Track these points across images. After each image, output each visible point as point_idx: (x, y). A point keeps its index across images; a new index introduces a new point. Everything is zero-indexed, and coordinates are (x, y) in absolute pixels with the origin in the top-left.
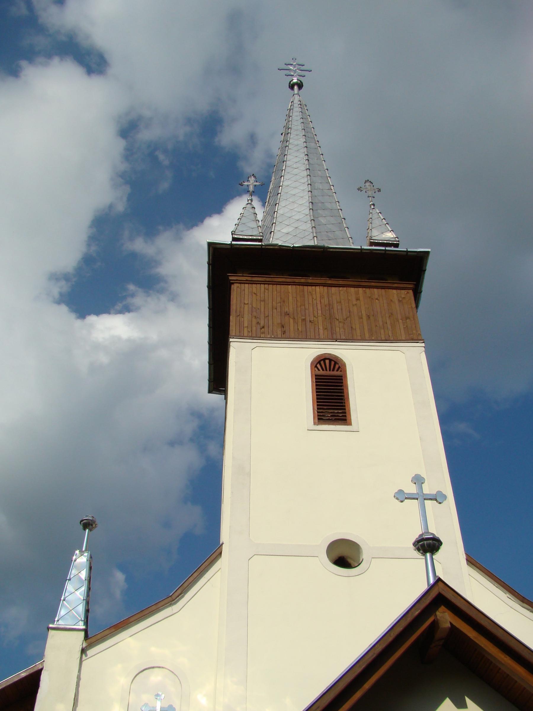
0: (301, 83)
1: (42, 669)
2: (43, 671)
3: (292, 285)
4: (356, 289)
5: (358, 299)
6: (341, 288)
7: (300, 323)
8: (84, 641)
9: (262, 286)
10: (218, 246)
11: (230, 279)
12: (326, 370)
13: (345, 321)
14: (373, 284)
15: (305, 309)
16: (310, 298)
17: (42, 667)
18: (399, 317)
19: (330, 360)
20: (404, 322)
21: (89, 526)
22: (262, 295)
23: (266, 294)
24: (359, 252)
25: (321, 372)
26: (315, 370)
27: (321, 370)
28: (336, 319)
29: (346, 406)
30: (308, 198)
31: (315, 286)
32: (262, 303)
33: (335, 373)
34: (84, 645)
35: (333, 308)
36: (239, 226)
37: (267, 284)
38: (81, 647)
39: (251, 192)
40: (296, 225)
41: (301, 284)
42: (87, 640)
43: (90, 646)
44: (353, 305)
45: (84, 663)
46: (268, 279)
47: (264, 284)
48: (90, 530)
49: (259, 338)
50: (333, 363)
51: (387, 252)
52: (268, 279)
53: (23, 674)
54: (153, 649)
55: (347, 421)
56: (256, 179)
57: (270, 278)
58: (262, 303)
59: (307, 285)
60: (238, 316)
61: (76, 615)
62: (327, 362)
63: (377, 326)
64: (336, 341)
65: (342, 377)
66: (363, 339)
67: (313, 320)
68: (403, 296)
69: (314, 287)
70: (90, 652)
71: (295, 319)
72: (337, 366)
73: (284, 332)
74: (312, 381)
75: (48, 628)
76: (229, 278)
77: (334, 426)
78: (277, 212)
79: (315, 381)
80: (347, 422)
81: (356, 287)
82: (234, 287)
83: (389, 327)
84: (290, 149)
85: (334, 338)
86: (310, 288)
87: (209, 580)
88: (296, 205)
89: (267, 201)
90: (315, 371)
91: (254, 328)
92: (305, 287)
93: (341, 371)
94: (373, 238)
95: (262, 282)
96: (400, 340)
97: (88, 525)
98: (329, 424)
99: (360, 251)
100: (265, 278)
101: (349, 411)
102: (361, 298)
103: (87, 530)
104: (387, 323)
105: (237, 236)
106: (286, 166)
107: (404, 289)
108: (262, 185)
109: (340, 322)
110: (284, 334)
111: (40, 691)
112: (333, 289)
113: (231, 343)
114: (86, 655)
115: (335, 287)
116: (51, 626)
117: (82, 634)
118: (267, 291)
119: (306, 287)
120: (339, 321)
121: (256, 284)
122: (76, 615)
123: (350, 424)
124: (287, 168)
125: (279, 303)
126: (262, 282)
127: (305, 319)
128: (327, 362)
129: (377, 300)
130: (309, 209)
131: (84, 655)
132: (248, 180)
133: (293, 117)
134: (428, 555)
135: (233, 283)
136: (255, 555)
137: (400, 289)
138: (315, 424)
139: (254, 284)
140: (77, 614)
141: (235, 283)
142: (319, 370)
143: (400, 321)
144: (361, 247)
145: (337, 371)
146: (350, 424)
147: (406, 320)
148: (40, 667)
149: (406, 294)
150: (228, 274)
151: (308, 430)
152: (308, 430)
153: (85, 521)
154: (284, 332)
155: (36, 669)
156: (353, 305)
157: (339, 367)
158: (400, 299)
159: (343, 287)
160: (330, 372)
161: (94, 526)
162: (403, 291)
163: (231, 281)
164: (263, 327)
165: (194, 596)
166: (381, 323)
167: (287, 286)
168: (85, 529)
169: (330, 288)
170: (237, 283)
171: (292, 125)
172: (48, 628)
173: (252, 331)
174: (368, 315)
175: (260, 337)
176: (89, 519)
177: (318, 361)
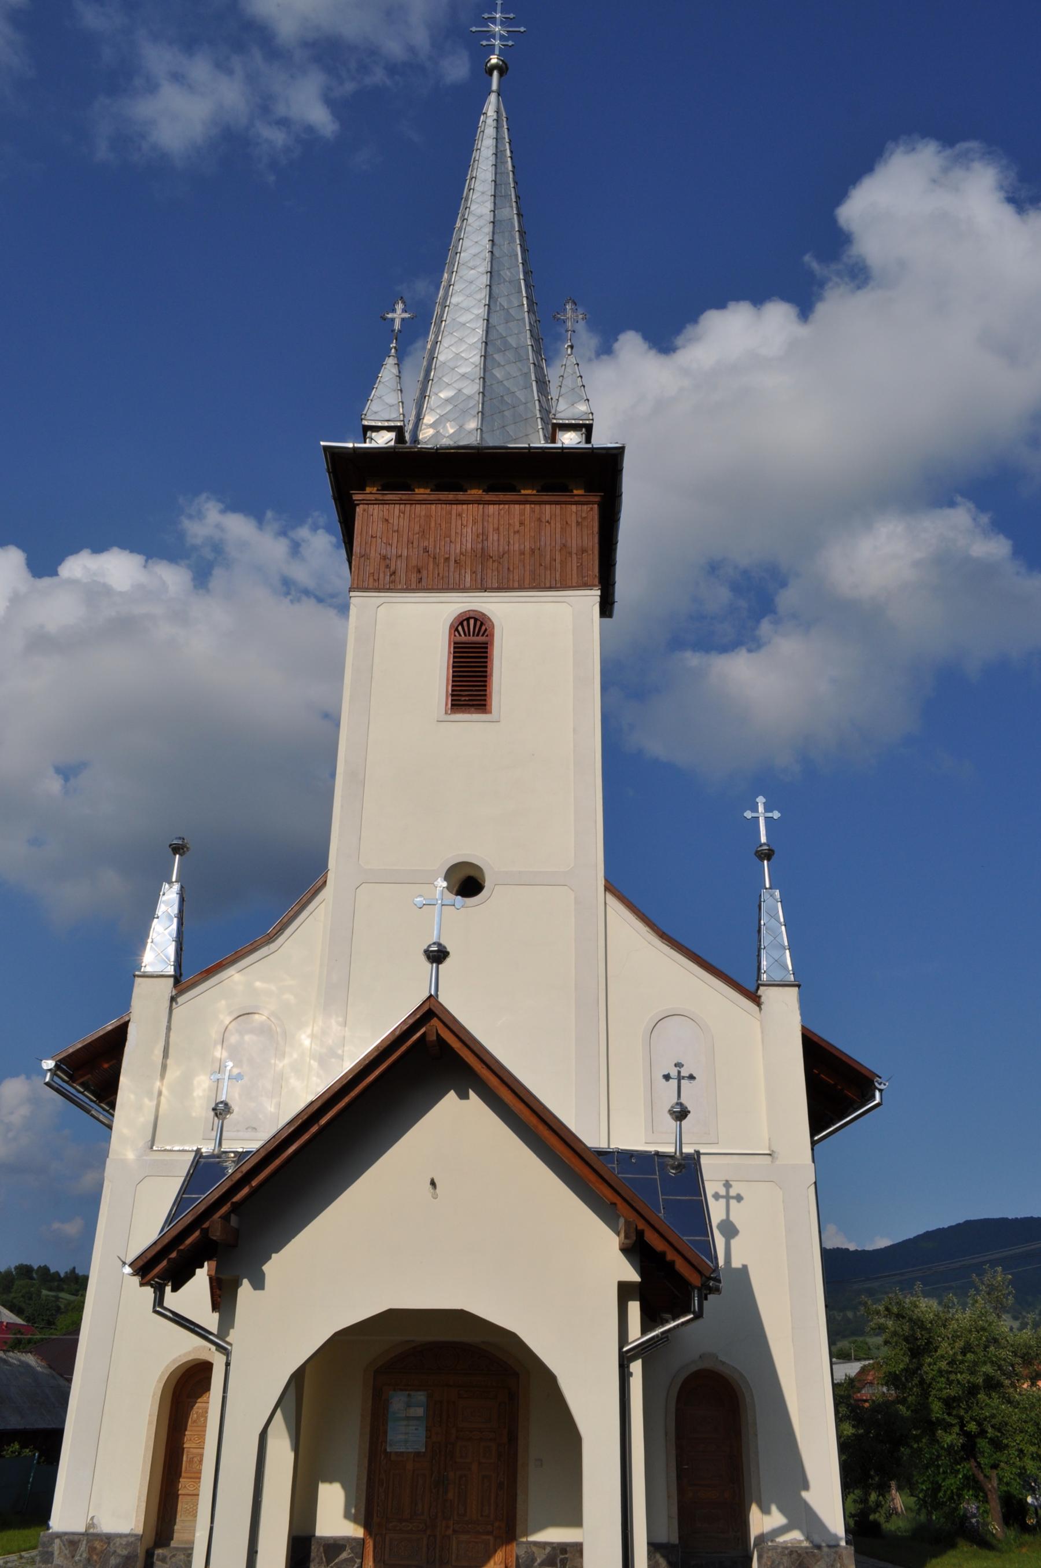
0: (504, 66)
1: (129, 1021)
2: (130, 1024)
3: (436, 504)
4: (522, 506)
5: (522, 523)
6: (502, 506)
7: (441, 565)
8: (173, 989)
9: (397, 506)
10: (336, 450)
11: (354, 498)
12: (469, 635)
13: (500, 558)
14: (545, 498)
15: (451, 542)
16: (459, 522)
17: (129, 1019)
18: (574, 550)
19: (476, 620)
20: (579, 557)
21: (179, 851)
22: (396, 522)
23: (401, 520)
24: (88, 1092)
25: (463, 638)
26: (455, 636)
27: (463, 635)
28: (490, 556)
29: (488, 686)
30: (481, 333)
31: (468, 504)
32: (396, 534)
33: (480, 639)
34: (174, 993)
35: (487, 539)
36: (373, 402)
37: (403, 504)
38: (170, 995)
39: (396, 331)
40: (458, 385)
41: (448, 502)
42: (178, 988)
43: (181, 993)
44: (515, 533)
45: (174, 1011)
46: (404, 497)
47: (400, 504)
48: (181, 855)
49: (390, 590)
50: (478, 623)
51: (565, 451)
52: (404, 497)
53: (109, 1026)
54: (258, 984)
55: (487, 707)
56: (405, 306)
57: (407, 495)
58: (396, 534)
59: (457, 504)
60: (363, 556)
61: (165, 959)
62: (472, 622)
63: (542, 565)
64: (485, 591)
65: (487, 644)
66: (521, 588)
67: (460, 560)
68: (584, 515)
69: (465, 507)
70: (180, 1000)
71: (435, 558)
72: (483, 628)
73: (420, 580)
74: (449, 652)
75: (135, 976)
76: (352, 498)
77: (469, 715)
78: (437, 358)
79: (452, 652)
80: (486, 709)
81: (523, 504)
82: (359, 510)
83: (558, 566)
84: (469, 225)
85: (482, 587)
86: (460, 507)
87: (311, 913)
88: (464, 347)
89: (434, 320)
90: (455, 638)
91: (381, 575)
92: (453, 506)
93: (487, 636)
94: (558, 416)
95: (397, 502)
96: (569, 587)
97: (177, 849)
98: (463, 712)
99: (527, 451)
100: (400, 496)
101: (491, 693)
102: (527, 522)
103: (177, 856)
104: (555, 560)
105: (368, 422)
106: (459, 263)
107: (587, 504)
108: (413, 319)
109: (494, 561)
110: (419, 582)
111: (127, 1044)
112: (491, 507)
113: (352, 598)
114: (177, 1003)
115: (494, 504)
116: (137, 973)
117: (172, 980)
118: (402, 515)
119: (454, 506)
120: (494, 559)
121: (389, 504)
122: (165, 959)
123: (490, 712)
124: (461, 267)
125: (417, 534)
126: (397, 502)
127: (449, 558)
128: (472, 622)
129: (547, 524)
130: (480, 355)
131: (174, 1003)
132: (393, 310)
133: (482, 149)
134: (434, 965)
135: (358, 505)
136: (364, 883)
137: (582, 504)
138: (446, 713)
139: (386, 504)
140: (533, 393)
141: (361, 504)
142: (460, 635)
143: (574, 556)
144: (529, 445)
145: (483, 635)
146: (490, 712)
147: (582, 554)
148: (127, 1019)
149: (589, 511)
150: (352, 492)
151: (438, 721)
152: (438, 721)
153: (174, 846)
154: (420, 580)
155: (122, 1021)
156: (515, 533)
157: (486, 630)
158: (580, 520)
159: (504, 504)
160: (473, 638)
161: (185, 849)
162: (585, 507)
163: (356, 502)
164: (394, 573)
165: (294, 932)
166: (548, 562)
167: (429, 506)
168: (175, 854)
169: (486, 506)
170: (363, 504)
171: (479, 169)
172: (135, 976)
173: (378, 579)
174: (533, 547)
175: (389, 589)
176: (179, 844)
177: (460, 621)
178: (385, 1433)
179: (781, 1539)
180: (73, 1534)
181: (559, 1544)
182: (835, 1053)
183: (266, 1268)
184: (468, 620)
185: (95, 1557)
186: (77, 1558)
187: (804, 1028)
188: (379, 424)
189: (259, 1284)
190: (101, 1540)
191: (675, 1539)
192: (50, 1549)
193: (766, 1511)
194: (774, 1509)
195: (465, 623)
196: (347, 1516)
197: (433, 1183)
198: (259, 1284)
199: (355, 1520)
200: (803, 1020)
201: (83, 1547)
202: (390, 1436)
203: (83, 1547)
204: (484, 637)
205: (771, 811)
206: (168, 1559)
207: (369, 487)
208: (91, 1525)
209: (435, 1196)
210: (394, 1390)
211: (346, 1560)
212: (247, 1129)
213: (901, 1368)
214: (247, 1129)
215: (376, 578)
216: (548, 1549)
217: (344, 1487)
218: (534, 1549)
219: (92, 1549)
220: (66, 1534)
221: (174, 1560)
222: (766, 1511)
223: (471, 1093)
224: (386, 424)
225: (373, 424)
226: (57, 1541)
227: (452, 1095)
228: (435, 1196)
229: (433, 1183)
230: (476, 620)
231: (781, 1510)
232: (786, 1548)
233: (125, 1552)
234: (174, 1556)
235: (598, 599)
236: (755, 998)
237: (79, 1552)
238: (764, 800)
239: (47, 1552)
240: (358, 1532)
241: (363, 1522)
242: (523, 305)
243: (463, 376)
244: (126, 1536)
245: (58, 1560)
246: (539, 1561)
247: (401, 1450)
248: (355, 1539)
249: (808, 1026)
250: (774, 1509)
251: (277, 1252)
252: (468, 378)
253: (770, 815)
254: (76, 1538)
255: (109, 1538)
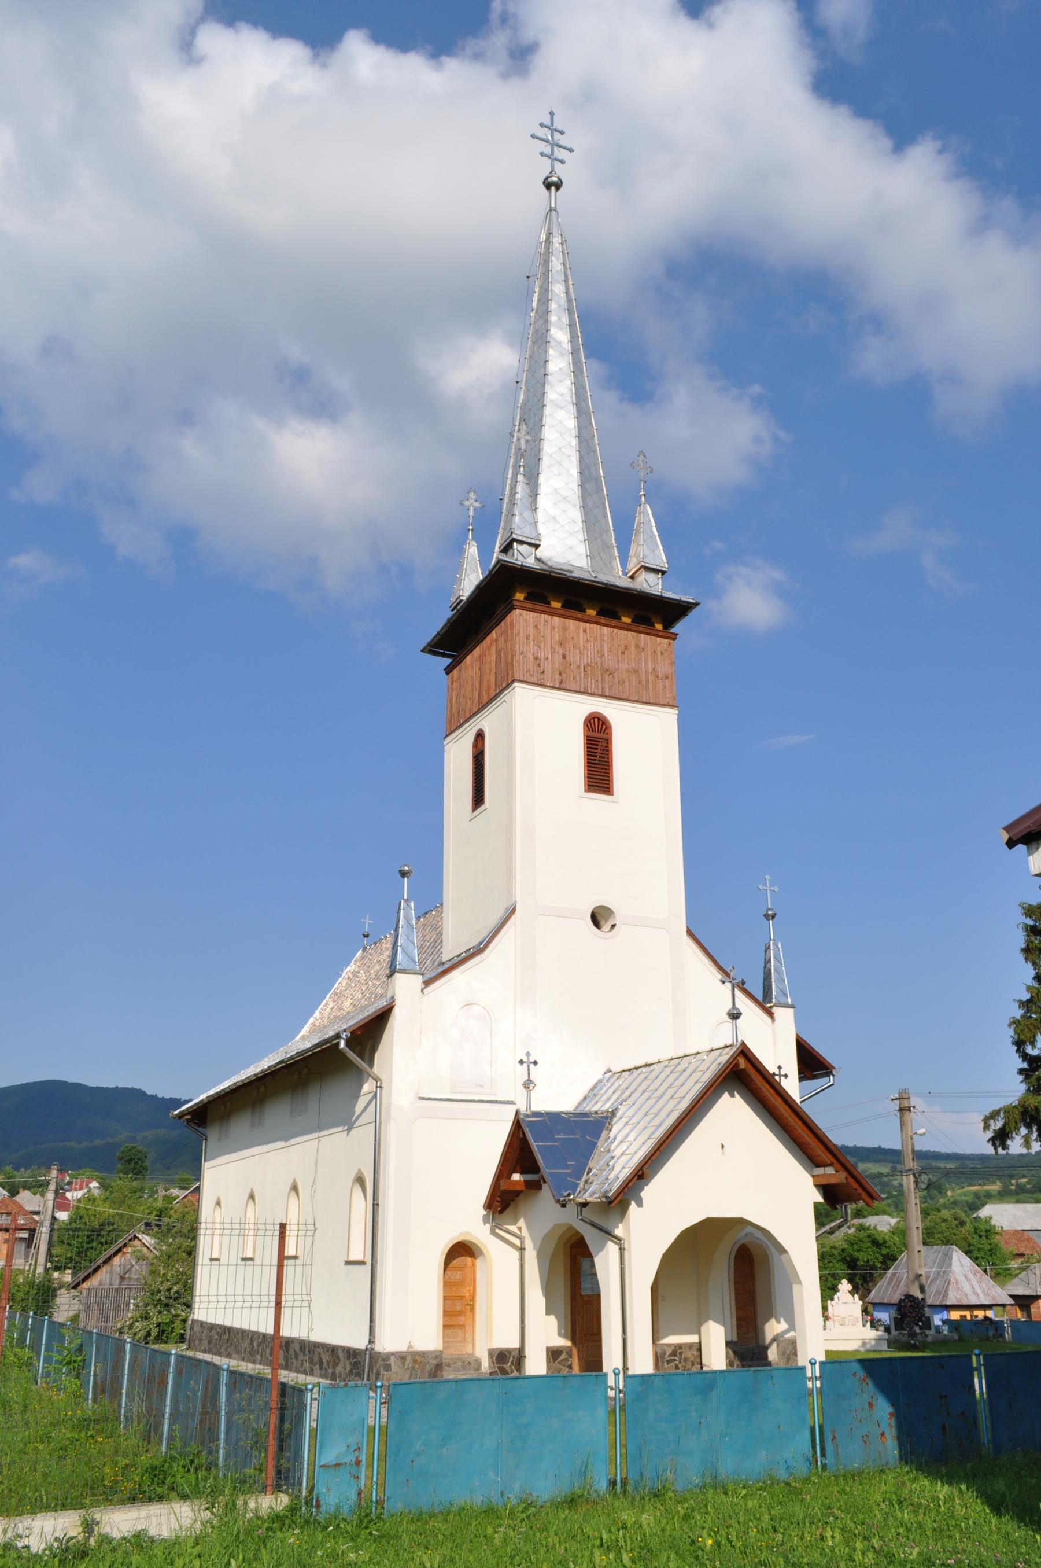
19: (599, 719)
48: (408, 877)
62: (596, 720)
72: (604, 727)
101: (612, 780)
178: (580, 1283)
179: (787, 1336)
180: (403, 1352)
181: (678, 1344)
182: (814, 1053)
183: (642, 1194)
184: (594, 719)
185: (417, 1366)
186: (406, 1367)
187: (797, 1035)
188: (524, 539)
189: (640, 1204)
190: (420, 1355)
191: (735, 1339)
192: (388, 1363)
193: (779, 1322)
194: (782, 1320)
195: (592, 721)
196: (560, 1334)
197: (723, 1146)
198: (640, 1204)
199: (565, 1336)
200: (796, 1029)
201: (409, 1359)
202: (583, 1283)
203: (409, 1359)
204: (605, 735)
205: (773, 886)
206: (451, 1365)
207: (520, 593)
208: (410, 1346)
209: (723, 1154)
210: (584, 1257)
211: (563, 1359)
212: (477, 1086)
213: (157, 1206)
214: (477, 1086)
215: (531, 673)
216: (673, 1347)
217: (557, 1317)
218: (665, 1348)
219: (415, 1361)
220: (397, 1352)
221: (455, 1365)
222: (779, 1322)
223: (736, 1094)
224: (529, 540)
225: (520, 538)
226: (392, 1357)
227: (726, 1095)
228: (723, 1154)
229: (723, 1146)
230: (599, 719)
231: (786, 1320)
232: (790, 1340)
233: (435, 1362)
234: (455, 1363)
235: (676, 717)
236: (771, 1014)
237: (407, 1364)
238: (769, 878)
239: (387, 1364)
240: (569, 1344)
241: (570, 1337)
242: (594, 436)
243: (565, 498)
244: (434, 1352)
245: (394, 1368)
246: (668, 1354)
247: (873, 1292)
248: (568, 1347)
249: (802, 1036)
250: (782, 1320)
251: (647, 1185)
252: (569, 502)
253: (773, 889)
254: (404, 1355)
255: (423, 1354)
